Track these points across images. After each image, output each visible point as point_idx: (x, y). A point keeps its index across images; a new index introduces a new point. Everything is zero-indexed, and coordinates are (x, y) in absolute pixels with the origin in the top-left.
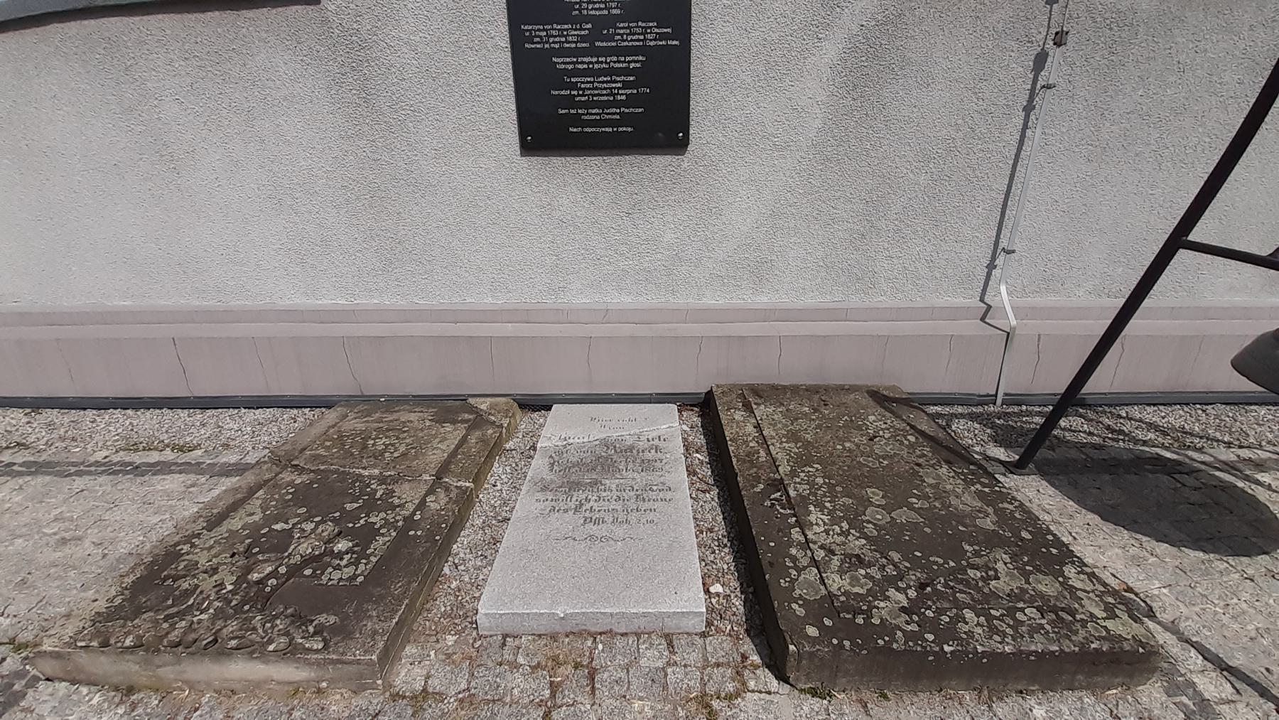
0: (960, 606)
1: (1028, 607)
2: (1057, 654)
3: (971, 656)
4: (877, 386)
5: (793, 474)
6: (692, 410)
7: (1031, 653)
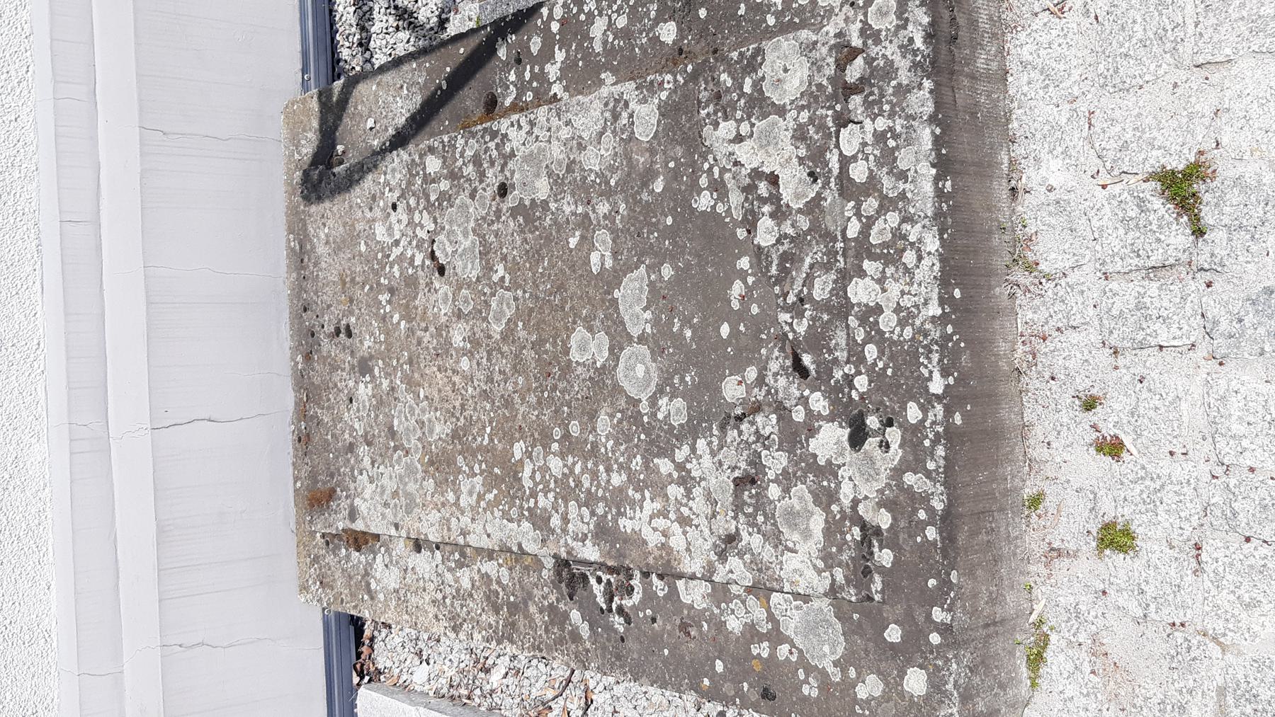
0: (840, 308)
1: (837, 146)
2: (938, 131)
3: (950, 329)
4: (289, 173)
5: (540, 521)
6: (372, 639)
7: (940, 194)
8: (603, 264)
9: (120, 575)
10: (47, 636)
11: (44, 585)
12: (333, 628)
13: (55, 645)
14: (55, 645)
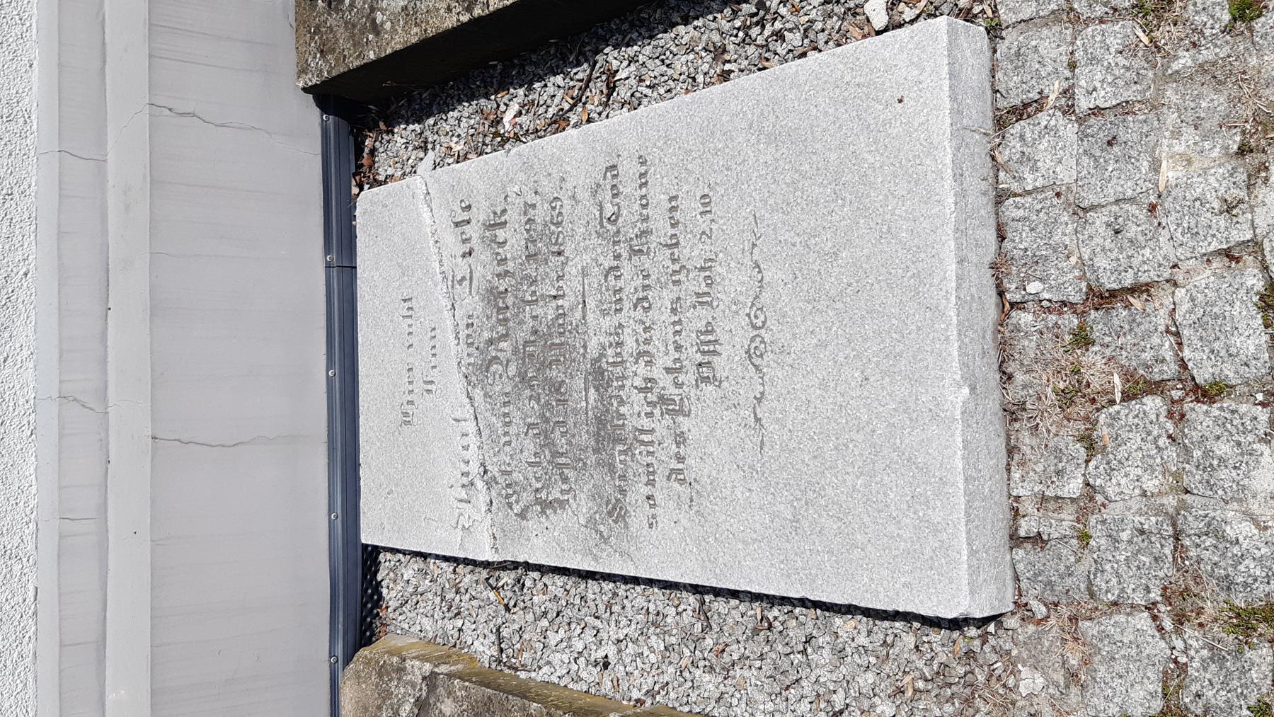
8: (1169, 380)
9: (108, 59)
10: (26, 116)
11: (26, 62)
12: (332, 135)
13: (35, 127)
14: (35, 127)
